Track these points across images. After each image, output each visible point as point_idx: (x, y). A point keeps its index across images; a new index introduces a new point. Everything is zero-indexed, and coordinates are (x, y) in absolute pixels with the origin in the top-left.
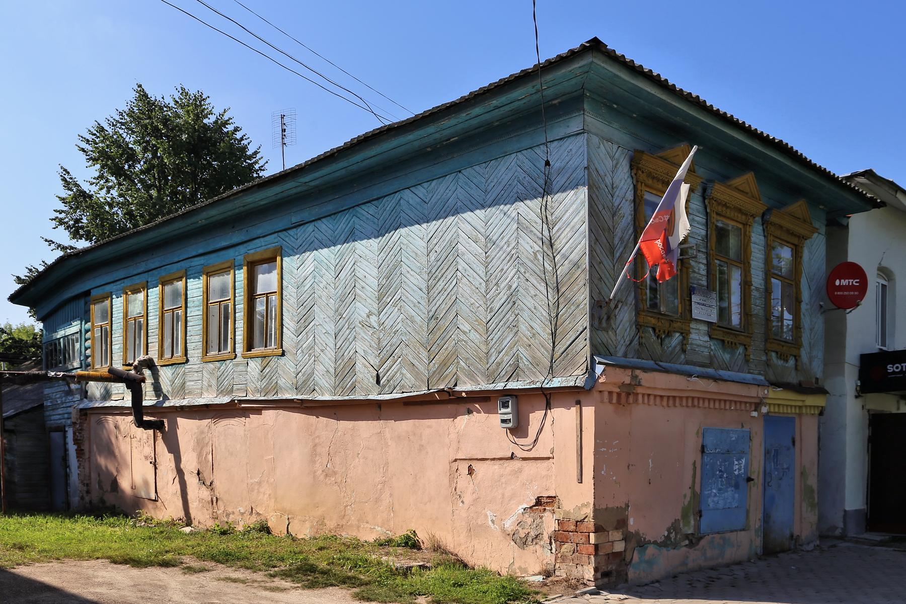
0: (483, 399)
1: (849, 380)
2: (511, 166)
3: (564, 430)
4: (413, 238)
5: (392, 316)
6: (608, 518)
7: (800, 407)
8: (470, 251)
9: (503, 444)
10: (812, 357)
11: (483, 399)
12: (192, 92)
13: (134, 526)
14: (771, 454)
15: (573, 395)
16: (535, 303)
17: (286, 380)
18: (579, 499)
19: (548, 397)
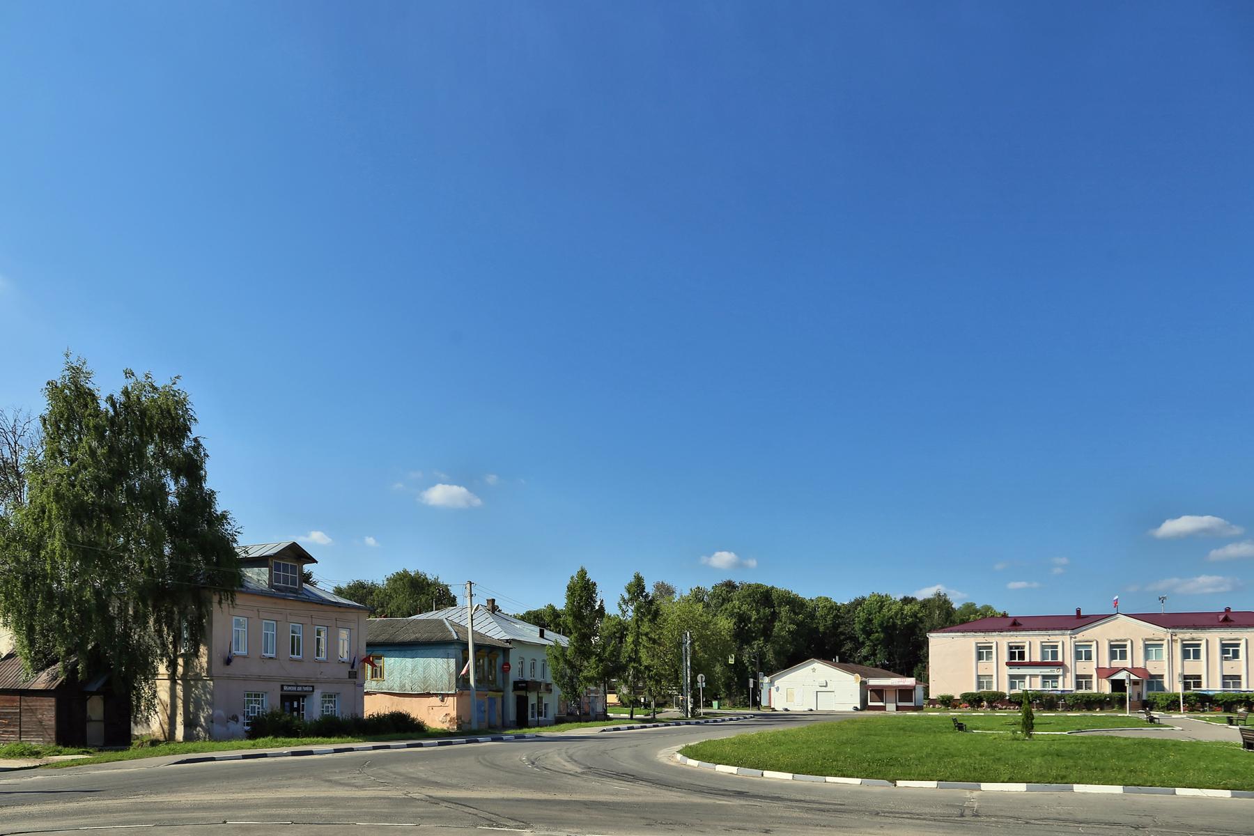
0: (436, 695)
1: (511, 687)
2: (441, 651)
3: (451, 702)
4: (421, 660)
5: (415, 676)
6: (459, 717)
7: (638, 635)
8: (433, 666)
9: (440, 704)
10: (500, 683)
11: (436, 695)
12: (107, 386)
13: (1117, 650)
14: (490, 706)
15: (452, 695)
16: (446, 677)
17: (385, 686)
18: (454, 714)
19: (448, 695)
